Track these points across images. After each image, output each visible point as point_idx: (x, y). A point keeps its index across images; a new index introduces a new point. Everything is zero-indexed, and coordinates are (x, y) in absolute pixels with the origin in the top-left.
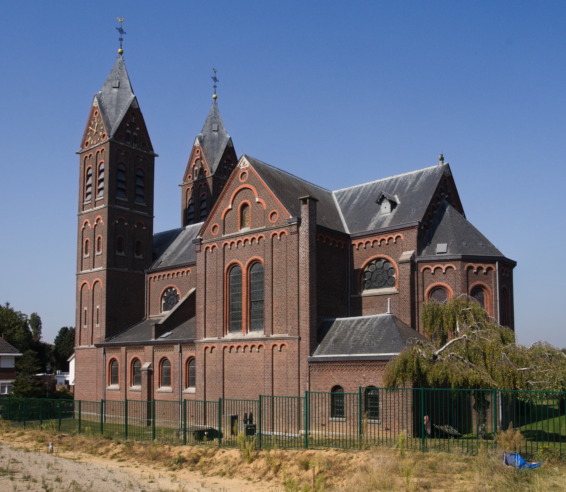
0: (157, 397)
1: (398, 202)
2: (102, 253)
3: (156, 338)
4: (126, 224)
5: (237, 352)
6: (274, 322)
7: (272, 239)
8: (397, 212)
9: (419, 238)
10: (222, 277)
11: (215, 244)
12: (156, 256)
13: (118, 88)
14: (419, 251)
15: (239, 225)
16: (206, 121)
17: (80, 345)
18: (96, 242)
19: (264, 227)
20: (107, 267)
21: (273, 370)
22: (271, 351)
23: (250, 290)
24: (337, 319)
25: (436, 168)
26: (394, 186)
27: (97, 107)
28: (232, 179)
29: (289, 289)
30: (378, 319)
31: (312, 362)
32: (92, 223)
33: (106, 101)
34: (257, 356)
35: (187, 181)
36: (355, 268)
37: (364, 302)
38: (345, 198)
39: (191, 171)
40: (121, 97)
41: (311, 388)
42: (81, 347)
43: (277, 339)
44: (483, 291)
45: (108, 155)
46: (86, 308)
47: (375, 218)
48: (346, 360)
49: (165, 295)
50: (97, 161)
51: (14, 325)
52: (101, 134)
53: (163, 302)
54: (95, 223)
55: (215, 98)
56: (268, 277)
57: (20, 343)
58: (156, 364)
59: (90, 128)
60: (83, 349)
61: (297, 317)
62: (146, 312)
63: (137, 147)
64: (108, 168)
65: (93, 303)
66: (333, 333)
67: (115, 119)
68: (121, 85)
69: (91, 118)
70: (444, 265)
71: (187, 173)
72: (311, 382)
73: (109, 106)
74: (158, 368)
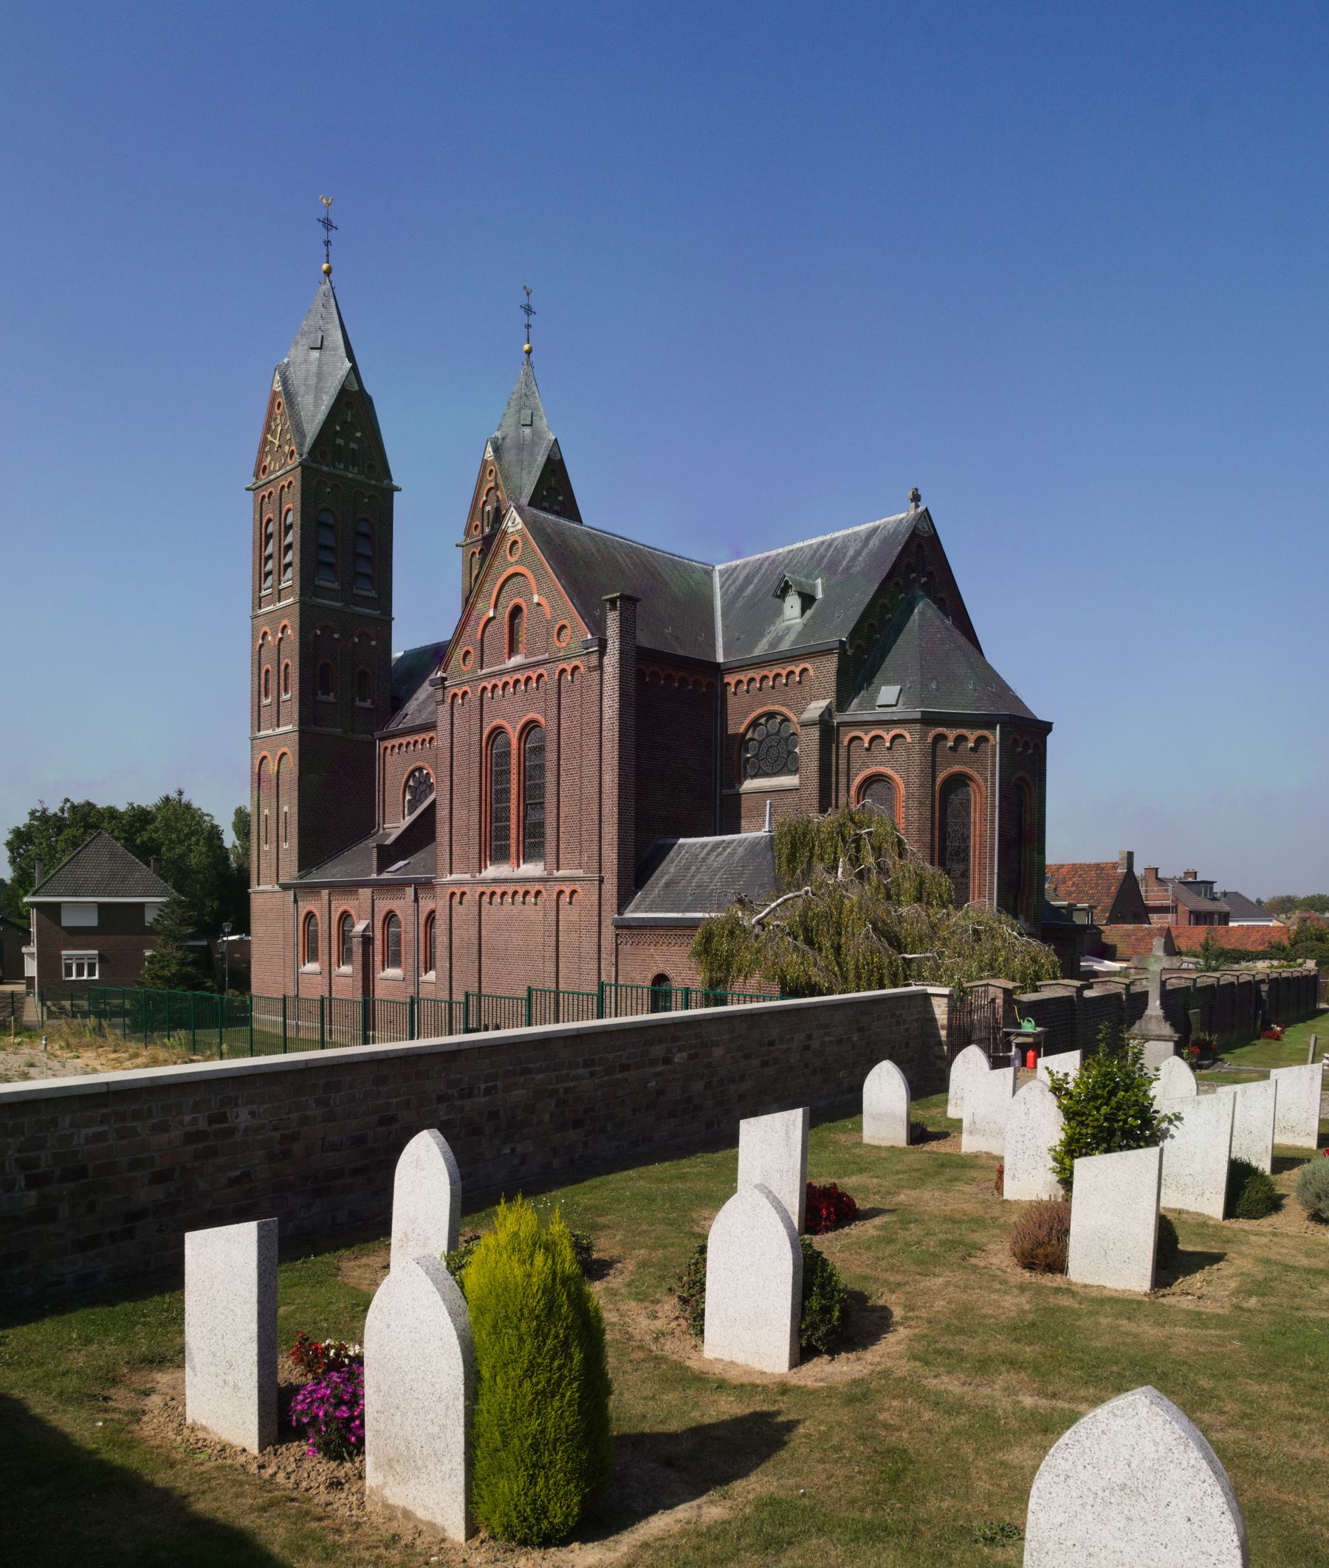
0: (380, 992)
1: (820, 595)
2: (290, 697)
3: (380, 871)
4: (336, 636)
5: (502, 904)
6: (562, 846)
7: (559, 680)
8: (812, 617)
9: (841, 672)
10: (478, 754)
11: (466, 688)
12: (397, 703)
13: (321, 348)
14: (842, 701)
15: (506, 651)
16: (509, 404)
17: (259, 884)
18: (282, 674)
19: (546, 656)
20: (300, 724)
21: (557, 941)
22: (554, 903)
23: (524, 782)
24: (681, 841)
25: (902, 519)
26: (823, 557)
27: (279, 392)
28: (495, 555)
29: (585, 781)
30: (746, 843)
31: (621, 926)
32: (274, 636)
33: (297, 379)
34: (534, 913)
35: (472, 536)
36: (730, 732)
37: (746, 804)
38: (734, 581)
39: (479, 514)
40: (325, 368)
41: (620, 978)
42: (262, 888)
43: (564, 879)
44: (968, 785)
45: (299, 495)
46: (266, 812)
47: (773, 628)
48: (674, 924)
49: (411, 783)
50: (280, 507)
51: (188, 836)
52: (287, 449)
53: (408, 797)
54: (280, 635)
55: (529, 352)
56: (551, 756)
57: (200, 873)
58: (378, 924)
59: (269, 436)
60: (263, 892)
61: (596, 838)
62: (378, 817)
63: (359, 473)
64: (299, 522)
65: (278, 801)
66: (668, 869)
67: (313, 416)
68: (325, 343)
69: (270, 416)
70: (888, 731)
71: (472, 518)
72: (620, 967)
73: (302, 390)
74: (380, 932)
